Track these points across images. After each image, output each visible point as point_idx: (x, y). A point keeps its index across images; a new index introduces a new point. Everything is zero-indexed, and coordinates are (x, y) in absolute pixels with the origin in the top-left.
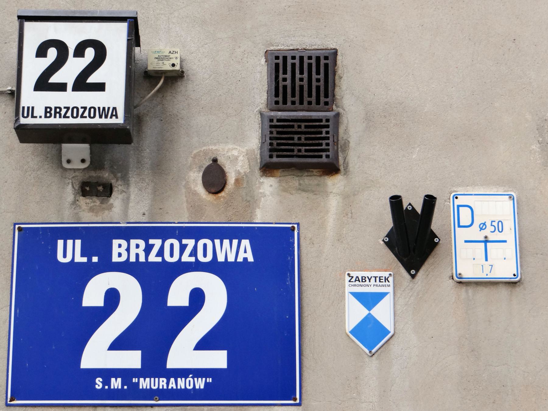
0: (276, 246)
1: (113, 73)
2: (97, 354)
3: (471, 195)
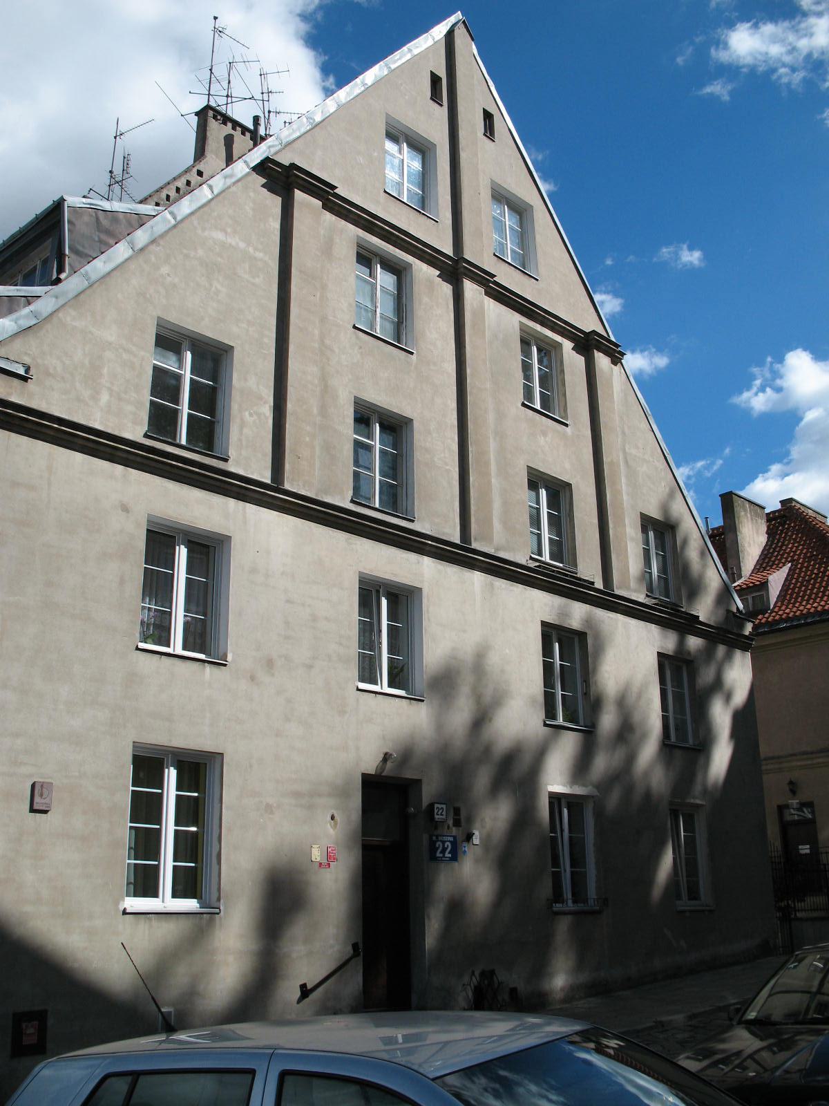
2: (438, 855)
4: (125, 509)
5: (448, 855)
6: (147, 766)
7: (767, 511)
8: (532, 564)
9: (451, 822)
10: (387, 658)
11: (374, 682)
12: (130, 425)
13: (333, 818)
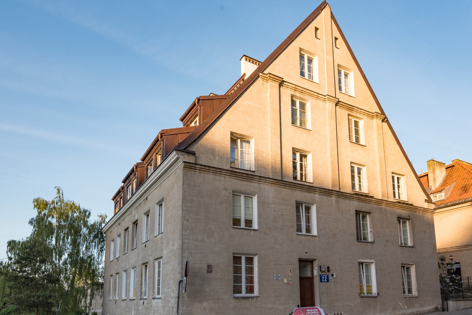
5: (326, 280)
6: (237, 259)
7: (446, 165)
8: (352, 193)
9: (326, 271)
11: (301, 232)
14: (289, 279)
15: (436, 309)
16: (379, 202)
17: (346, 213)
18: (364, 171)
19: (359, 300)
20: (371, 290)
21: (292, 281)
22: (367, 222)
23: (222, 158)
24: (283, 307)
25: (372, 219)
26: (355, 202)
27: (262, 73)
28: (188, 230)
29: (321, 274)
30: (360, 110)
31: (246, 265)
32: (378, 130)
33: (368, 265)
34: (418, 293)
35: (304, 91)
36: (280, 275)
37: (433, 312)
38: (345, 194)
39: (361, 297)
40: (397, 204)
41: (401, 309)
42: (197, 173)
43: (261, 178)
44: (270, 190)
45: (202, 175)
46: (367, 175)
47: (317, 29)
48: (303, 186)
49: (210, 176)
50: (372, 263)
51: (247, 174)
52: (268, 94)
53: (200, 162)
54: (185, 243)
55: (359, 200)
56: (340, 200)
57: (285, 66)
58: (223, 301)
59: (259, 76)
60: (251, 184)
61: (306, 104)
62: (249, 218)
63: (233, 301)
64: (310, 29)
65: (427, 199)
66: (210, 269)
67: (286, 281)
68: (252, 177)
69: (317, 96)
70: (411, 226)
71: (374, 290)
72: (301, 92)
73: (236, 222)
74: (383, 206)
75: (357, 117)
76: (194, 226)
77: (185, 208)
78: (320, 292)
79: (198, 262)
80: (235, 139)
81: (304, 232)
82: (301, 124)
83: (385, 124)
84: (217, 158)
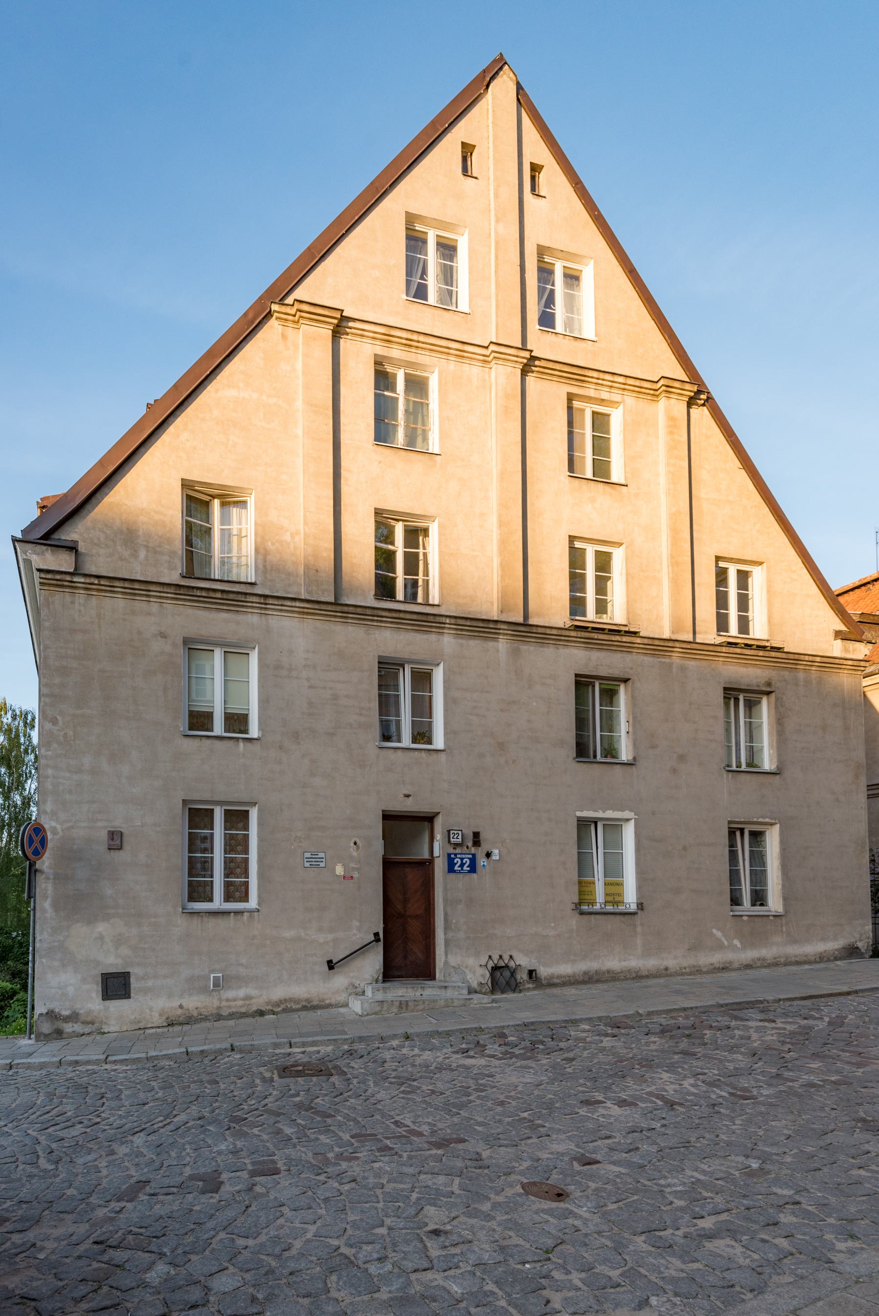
0: (474, 855)
1: (460, 837)
2: (456, 868)
3: (16, 553)
4: (163, 635)
6: (198, 817)
9: (470, 844)
10: (396, 544)
12: (166, 571)
13: (355, 843)
14: (353, 865)
15: (852, 952)
16: (659, 647)
17: (544, 684)
18: (618, 558)
19: (574, 921)
20: (621, 895)
21: (358, 869)
22: (761, 718)
23: (156, 552)
24: (330, 937)
25: (633, 697)
26: (575, 651)
27: (281, 302)
28: (55, 745)
29: (451, 851)
30: (608, 377)
31: (226, 829)
32: (671, 433)
33: (614, 827)
34: (785, 905)
35: (414, 340)
36: (321, 855)
37: (836, 959)
38: (540, 630)
39: (582, 913)
40: (724, 649)
41: (720, 947)
42: (81, 597)
43: (268, 601)
44: (296, 633)
45: (94, 601)
46: (624, 571)
47: (467, 150)
48: (402, 615)
49: (116, 604)
50: (628, 820)
51: (223, 591)
52: (299, 366)
53: (92, 568)
54: (47, 777)
55: (589, 644)
56: (524, 648)
57: (362, 275)
58: (153, 920)
59: (269, 315)
60: (240, 617)
61: (427, 379)
62: (236, 708)
63: (181, 922)
64: (448, 150)
65: (843, 628)
66: (116, 840)
67: (339, 870)
68: (240, 597)
69: (460, 350)
70: (773, 710)
71: (630, 896)
72: (408, 345)
73: (200, 721)
74: (676, 658)
75: (602, 402)
76: (71, 733)
77: (45, 691)
78: (445, 900)
79: (83, 824)
80: (197, 501)
81: (406, 740)
82: (411, 440)
83: (700, 414)
84: (142, 554)
